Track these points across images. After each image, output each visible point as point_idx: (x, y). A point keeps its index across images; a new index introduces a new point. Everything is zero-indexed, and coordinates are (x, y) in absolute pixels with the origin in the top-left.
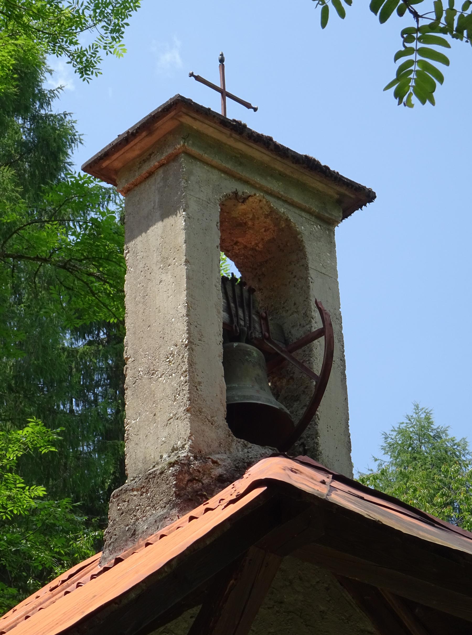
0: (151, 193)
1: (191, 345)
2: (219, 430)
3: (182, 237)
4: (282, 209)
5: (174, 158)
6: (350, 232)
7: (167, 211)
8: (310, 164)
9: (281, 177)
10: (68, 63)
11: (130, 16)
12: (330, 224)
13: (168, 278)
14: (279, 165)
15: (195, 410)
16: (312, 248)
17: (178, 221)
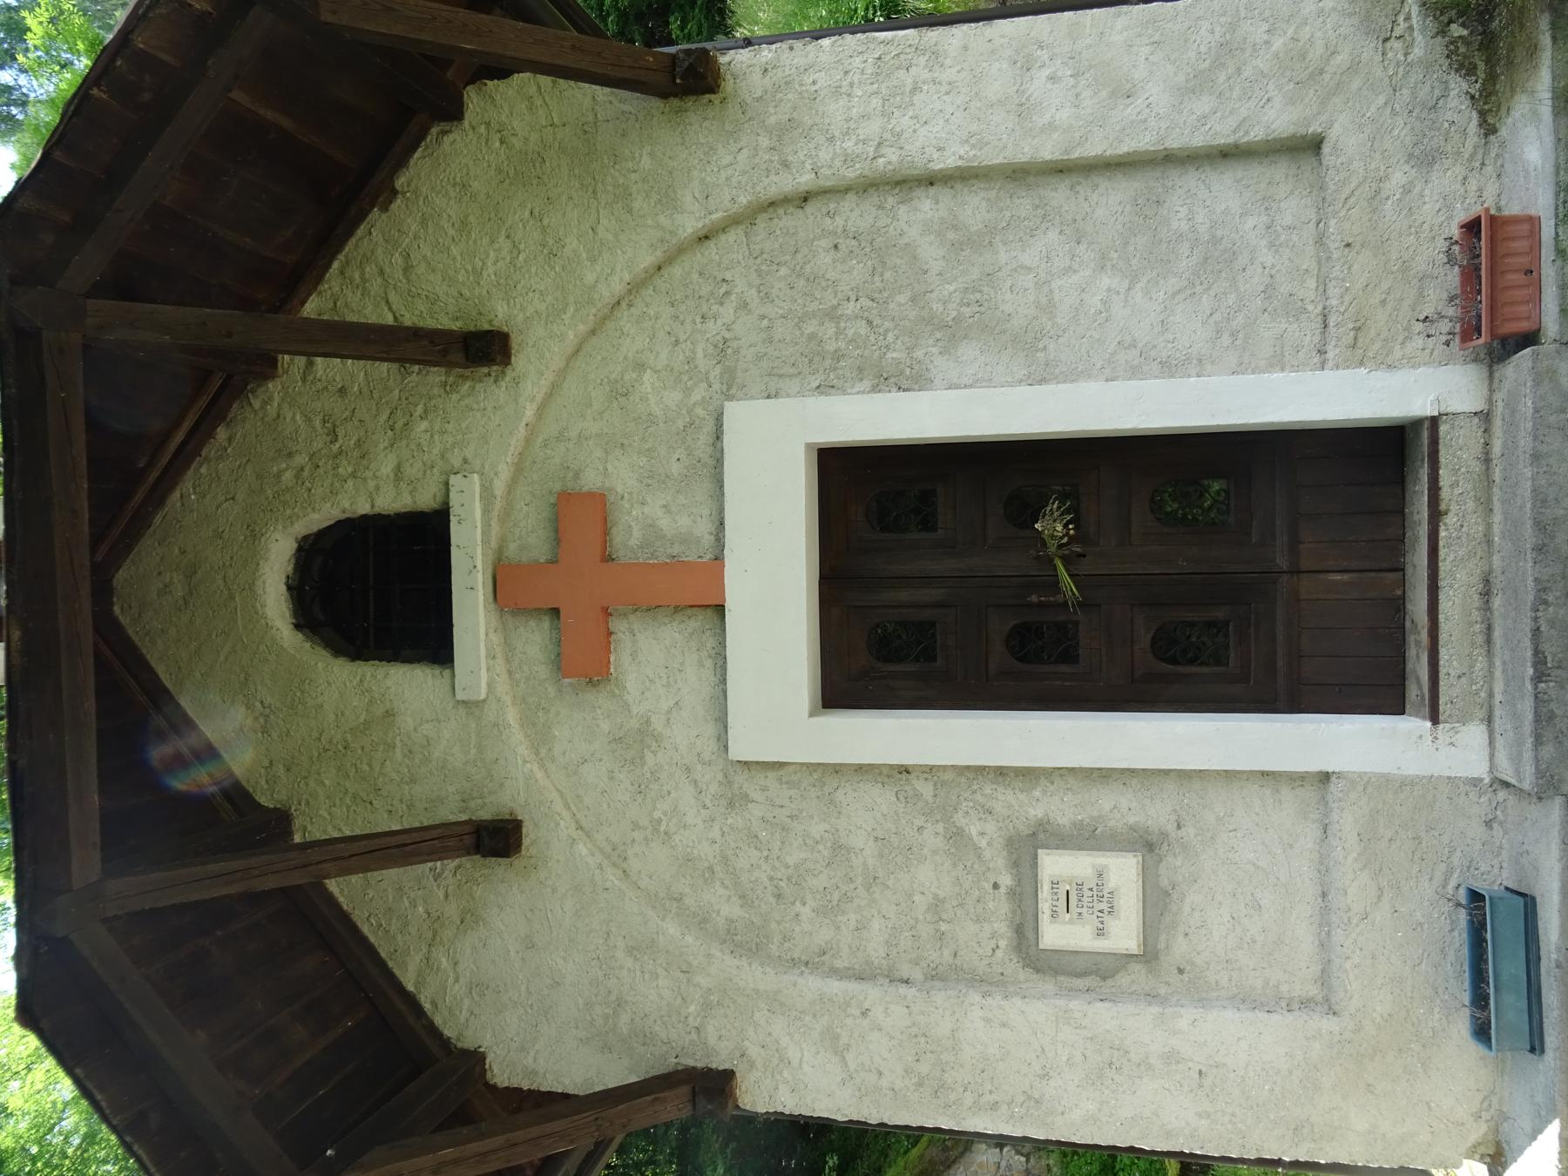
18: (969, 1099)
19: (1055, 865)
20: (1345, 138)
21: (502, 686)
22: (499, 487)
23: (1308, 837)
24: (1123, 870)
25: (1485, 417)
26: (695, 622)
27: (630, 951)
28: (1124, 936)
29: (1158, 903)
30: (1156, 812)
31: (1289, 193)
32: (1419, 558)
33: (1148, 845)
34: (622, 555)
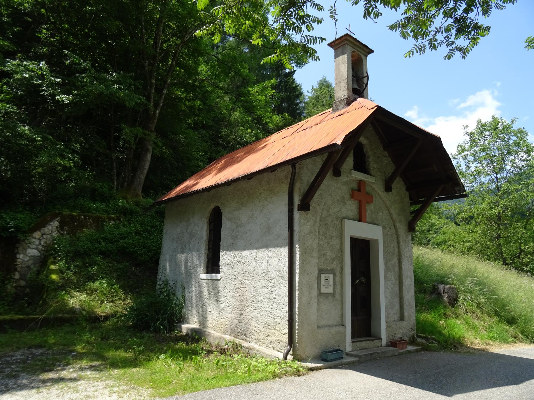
0: (340, 50)
1: (348, 78)
2: (351, 93)
3: (346, 59)
4: (360, 54)
5: (345, 44)
6: (370, 57)
7: (343, 54)
8: (365, 46)
9: (360, 48)
10: (449, 57)
11: (367, 19)
12: (366, 56)
13: (343, 66)
14: (360, 46)
15: (348, 89)
16: (364, 61)
17: (346, 56)
18: (304, 259)
19: (331, 276)
20: (404, 324)
21: (352, 178)
22: (373, 185)
23: (335, 323)
24: (330, 290)
25: (381, 346)
26: (358, 217)
27: (321, 194)
28: (324, 290)
29: (327, 296)
30: (338, 296)
31: (397, 317)
32: (367, 338)
33: (333, 295)
34: (357, 202)
